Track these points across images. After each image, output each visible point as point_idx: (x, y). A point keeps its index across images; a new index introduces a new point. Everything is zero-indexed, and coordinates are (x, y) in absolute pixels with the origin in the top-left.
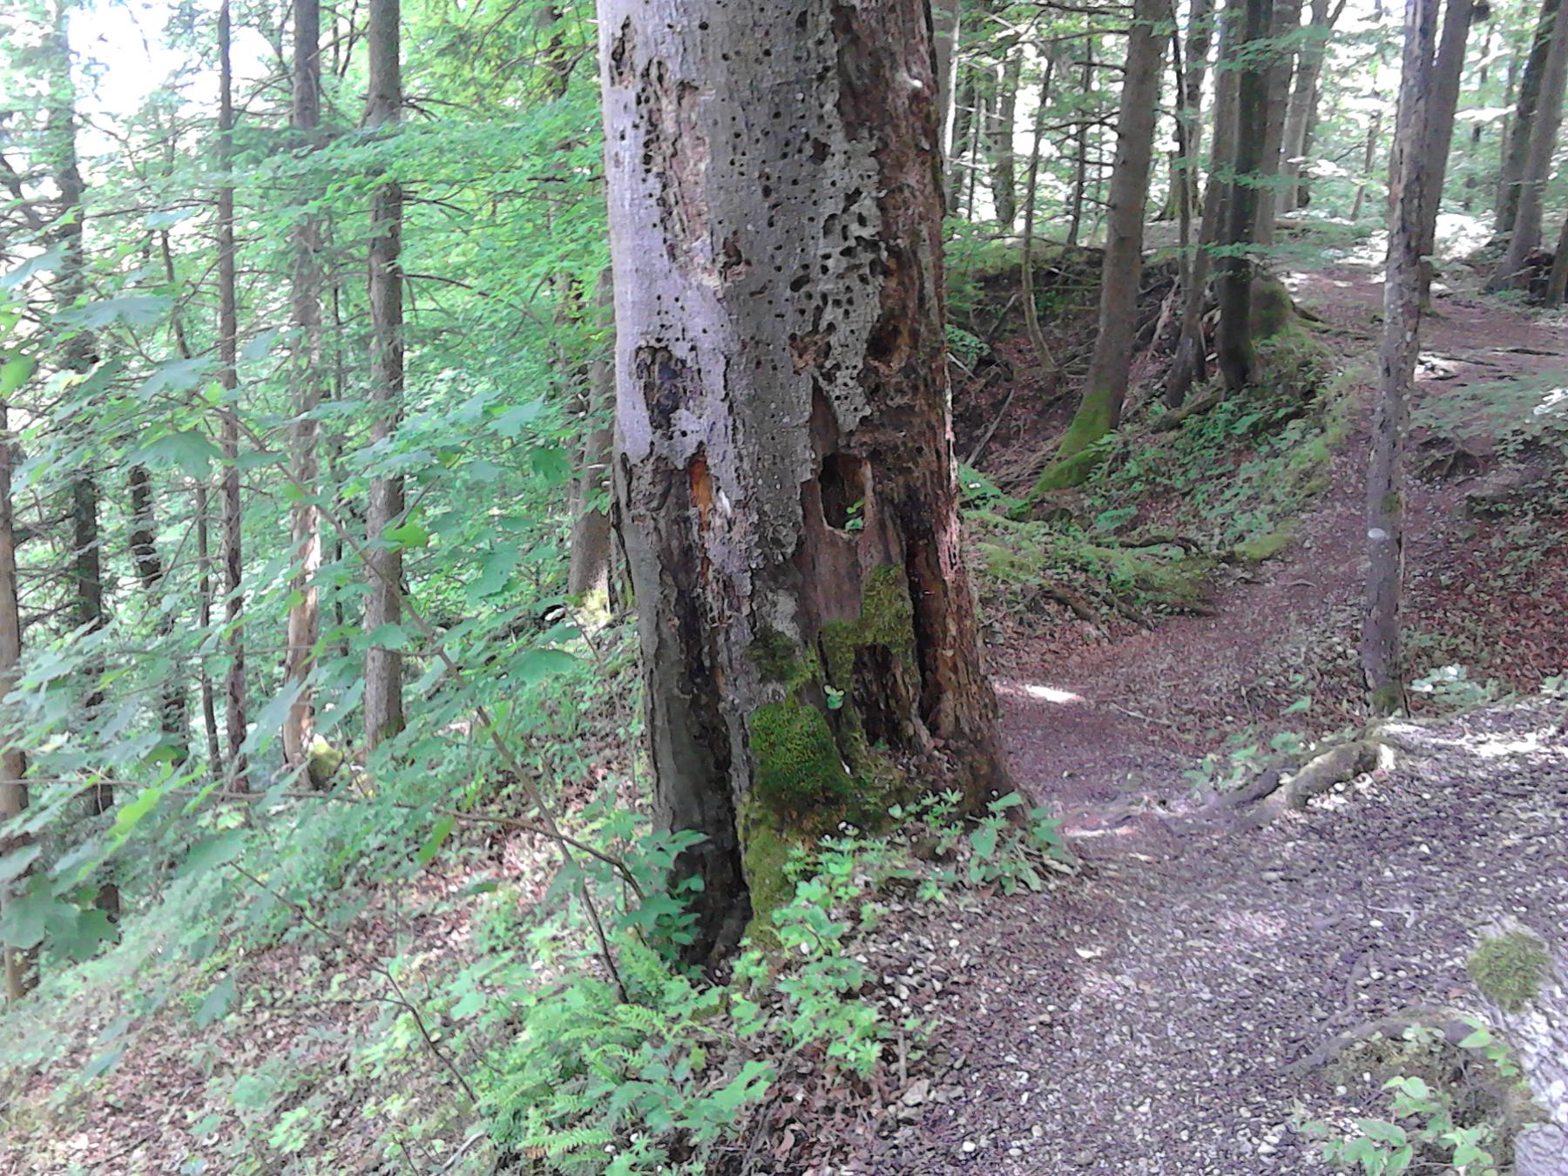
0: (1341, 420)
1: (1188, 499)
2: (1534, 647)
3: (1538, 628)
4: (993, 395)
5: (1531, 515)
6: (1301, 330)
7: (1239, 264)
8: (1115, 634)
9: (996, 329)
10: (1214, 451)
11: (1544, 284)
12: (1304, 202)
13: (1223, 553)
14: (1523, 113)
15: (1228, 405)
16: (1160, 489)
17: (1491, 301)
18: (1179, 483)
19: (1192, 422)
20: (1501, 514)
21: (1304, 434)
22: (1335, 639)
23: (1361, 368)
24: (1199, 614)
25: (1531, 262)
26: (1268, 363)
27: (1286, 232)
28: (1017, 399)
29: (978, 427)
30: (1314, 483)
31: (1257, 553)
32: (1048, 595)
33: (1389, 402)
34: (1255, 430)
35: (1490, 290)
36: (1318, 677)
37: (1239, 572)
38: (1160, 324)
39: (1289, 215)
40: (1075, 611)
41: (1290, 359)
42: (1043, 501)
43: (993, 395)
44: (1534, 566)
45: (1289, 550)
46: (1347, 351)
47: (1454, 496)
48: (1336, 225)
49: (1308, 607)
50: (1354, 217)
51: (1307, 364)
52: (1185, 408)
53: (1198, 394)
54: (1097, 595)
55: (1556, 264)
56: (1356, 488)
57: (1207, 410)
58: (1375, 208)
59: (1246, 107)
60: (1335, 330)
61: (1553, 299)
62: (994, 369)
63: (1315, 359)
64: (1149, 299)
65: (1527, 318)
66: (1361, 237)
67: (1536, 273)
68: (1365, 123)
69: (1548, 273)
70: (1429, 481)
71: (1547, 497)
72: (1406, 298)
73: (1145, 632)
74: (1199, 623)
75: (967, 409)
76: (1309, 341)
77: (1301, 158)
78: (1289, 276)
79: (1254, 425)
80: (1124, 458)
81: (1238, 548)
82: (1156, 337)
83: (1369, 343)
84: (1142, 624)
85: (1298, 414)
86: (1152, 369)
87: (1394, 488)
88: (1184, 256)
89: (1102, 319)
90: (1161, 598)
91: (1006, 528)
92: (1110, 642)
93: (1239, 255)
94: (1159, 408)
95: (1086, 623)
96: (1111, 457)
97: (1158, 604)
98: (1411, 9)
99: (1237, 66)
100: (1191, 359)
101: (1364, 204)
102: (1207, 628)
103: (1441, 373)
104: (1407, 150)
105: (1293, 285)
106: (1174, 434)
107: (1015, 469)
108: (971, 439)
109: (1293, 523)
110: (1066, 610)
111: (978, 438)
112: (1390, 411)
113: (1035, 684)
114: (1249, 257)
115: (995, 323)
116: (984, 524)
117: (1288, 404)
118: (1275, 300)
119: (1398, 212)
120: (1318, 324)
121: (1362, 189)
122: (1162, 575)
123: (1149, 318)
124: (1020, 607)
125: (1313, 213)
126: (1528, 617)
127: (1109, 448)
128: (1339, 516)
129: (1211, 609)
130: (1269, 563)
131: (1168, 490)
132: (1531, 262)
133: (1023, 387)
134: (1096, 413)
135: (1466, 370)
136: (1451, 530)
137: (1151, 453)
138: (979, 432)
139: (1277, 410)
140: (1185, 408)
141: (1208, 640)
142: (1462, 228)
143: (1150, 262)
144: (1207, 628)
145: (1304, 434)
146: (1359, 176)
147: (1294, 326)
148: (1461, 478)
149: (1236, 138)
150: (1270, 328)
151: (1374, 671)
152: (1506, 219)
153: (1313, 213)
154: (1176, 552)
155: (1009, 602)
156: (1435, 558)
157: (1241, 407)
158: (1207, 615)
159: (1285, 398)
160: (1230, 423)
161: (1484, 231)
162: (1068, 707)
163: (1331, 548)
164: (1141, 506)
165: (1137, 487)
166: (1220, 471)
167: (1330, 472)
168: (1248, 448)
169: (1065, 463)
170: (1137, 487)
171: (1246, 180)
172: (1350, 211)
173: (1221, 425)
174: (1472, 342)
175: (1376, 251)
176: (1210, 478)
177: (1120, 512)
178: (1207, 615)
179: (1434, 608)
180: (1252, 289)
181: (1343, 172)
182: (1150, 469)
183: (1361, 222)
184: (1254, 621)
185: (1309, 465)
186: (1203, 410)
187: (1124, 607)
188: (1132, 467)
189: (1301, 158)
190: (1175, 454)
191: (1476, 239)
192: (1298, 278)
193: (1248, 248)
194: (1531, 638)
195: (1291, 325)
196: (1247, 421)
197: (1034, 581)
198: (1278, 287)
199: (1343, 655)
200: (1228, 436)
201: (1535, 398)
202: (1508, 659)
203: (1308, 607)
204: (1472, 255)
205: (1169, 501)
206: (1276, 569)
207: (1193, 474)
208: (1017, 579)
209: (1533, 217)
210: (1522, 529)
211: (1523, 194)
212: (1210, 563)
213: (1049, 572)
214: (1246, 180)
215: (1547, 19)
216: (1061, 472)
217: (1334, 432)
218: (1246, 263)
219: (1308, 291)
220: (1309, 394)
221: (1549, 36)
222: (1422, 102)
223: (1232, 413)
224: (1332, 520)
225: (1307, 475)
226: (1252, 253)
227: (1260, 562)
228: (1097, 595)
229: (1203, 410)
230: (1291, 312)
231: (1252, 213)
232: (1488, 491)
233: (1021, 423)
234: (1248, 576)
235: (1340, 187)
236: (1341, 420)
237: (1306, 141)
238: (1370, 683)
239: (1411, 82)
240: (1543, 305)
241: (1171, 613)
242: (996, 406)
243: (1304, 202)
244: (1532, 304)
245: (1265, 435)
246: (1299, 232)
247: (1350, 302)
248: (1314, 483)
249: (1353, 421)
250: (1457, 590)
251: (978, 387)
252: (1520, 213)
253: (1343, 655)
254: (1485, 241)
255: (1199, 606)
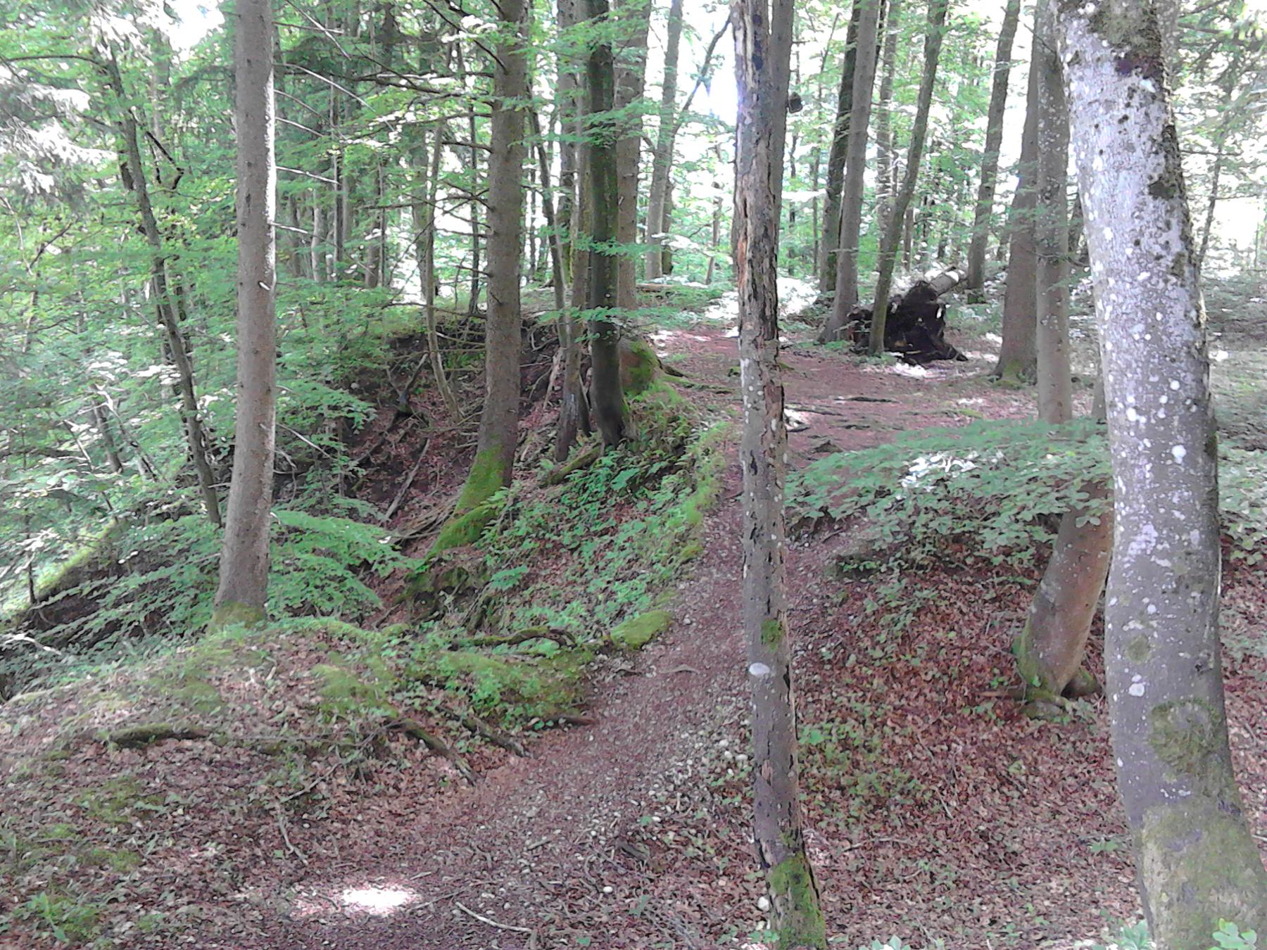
0: (710, 480)
1: (576, 554)
2: (920, 722)
3: (921, 698)
4: (411, 444)
5: (897, 571)
6: (668, 386)
7: (604, 328)
8: (477, 768)
9: (411, 385)
10: (598, 505)
11: (864, 335)
12: (668, 270)
13: (601, 642)
14: (833, 195)
15: (607, 461)
16: (549, 545)
17: (824, 351)
18: (566, 538)
19: (577, 476)
20: (869, 572)
21: (676, 491)
22: (723, 743)
23: (723, 423)
24: (576, 723)
25: (853, 317)
26: (641, 419)
27: (654, 295)
28: (434, 447)
29: (399, 474)
30: (691, 547)
31: (637, 638)
32: (394, 727)
33: (759, 507)
34: (633, 484)
35: (822, 341)
36: (708, 798)
37: (619, 663)
38: (553, 377)
39: (657, 280)
40: (429, 745)
41: (659, 414)
42: (440, 560)
43: (411, 444)
44: (908, 628)
45: (669, 629)
46: (710, 406)
47: (824, 554)
48: (694, 288)
49: (692, 701)
50: (708, 281)
51: (675, 419)
52: (570, 462)
53: (583, 448)
54: (457, 718)
55: (874, 317)
56: (730, 550)
57: (588, 465)
58: (723, 274)
59: (598, 180)
60: (697, 385)
61: (875, 348)
62: (411, 421)
63: (682, 415)
64: (541, 356)
65: (856, 365)
66: (714, 298)
67: (857, 327)
68: (712, 209)
69: (867, 326)
70: (798, 539)
71: (908, 552)
72: (767, 376)
73: (513, 760)
74: (575, 736)
75: (389, 458)
76: (676, 397)
77: (661, 235)
78: (656, 333)
79: (632, 480)
80: (515, 514)
81: (617, 631)
82: (550, 388)
83: (728, 396)
84: (509, 748)
85: (671, 469)
86: (548, 418)
87: (774, 611)
88: (561, 319)
89: (489, 379)
90: (531, 712)
91: (353, 640)
92: (470, 783)
93: (602, 317)
94: (547, 464)
95: (442, 760)
96: (503, 513)
97: (528, 719)
98: (740, 34)
99: (582, 139)
100: (574, 413)
101: (715, 271)
102: (585, 744)
103: (796, 425)
104: (750, 201)
105: (661, 341)
106: (561, 488)
107: (434, 511)
108: (393, 485)
109: (671, 594)
110: (417, 746)
111: (400, 484)
112: (760, 517)
113: (358, 885)
114: (614, 320)
115: (410, 379)
116: (327, 637)
117: (661, 459)
118: (641, 358)
119: (747, 276)
120: (683, 380)
121: (712, 259)
122: (532, 683)
123: (543, 372)
124: (357, 754)
125: (676, 279)
126: (910, 688)
127: (501, 505)
128: (717, 583)
129: (589, 717)
130: (649, 647)
131: (558, 546)
132: (853, 317)
133: (438, 436)
134: (489, 470)
135: (817, 421)
136: (825, 593)
137: (539, 509)
138: (400, 479)
139: (652, 464)
140: (570, 462)
141: (585, 760)
142: (794, 289)
143: (540, 323)
144: (585, 744)
145: (676, 491)
146: (709, 249)
147: (662, 382)
148: (827, 535)
149: (591, 209)
150: (640, 384)
151: (772, 844)
152: (828, 282)
153: (676, 279)
154: (547, 646)
155: (343, 748)
156: (813, 627)
157: (619, 461)
158: (584, 723)
159: (658, 452)
160: (610, 478)
161: (812, 292)
162: (406, 916)
163: (712, 622)
164: (532, 564)
165: (528, 545)
166: (604, 526)
167: (705, 535)
168: (628, 502)
169: (462, 519)
170: (528, 545)
171: (603, 247)
172: (705, 277)
173: (602, 478)
174: (817, 392)
175: (729, 308)
176: (595, 534)
177: (512, 572)
178: (584, 723)
179: (818, 689)
180: (619, 351)
181: (695, 245)
182: (539, 525)
183: (713, 285)
184: (636, 725)
185: (683, 528)
186: (586, 465)
187: (488, 730)
188: (522, 527)
189: (661, 235)
190: (562, 509)
191: (805, 298)
192: (664, 335)
193: (610, 312)
194: (916, 711)
195: (659, 381)
196: (624, 476)
197: (378, 714)
198: (643, 345)
199: (733, 764)
200: (609, 490)
201: (901, 469)
202: (899, 740)
203: (692, 701)
204: (804, 311)
205: (559, 557)
206: (657, 653)
207: (580, 531)
208: (356, 713)
209: (850, 280)
210: (891, 588)
211: (840, 260)
212: (587, 656)
213: (399, 697)
214: (603, 247)
215: (842, 119)
216: (458, 530)
217: (704, 492)
218: (611, 327)
219: (675, 348)
220: (679, 448)
221: (845, 133)
222: (762, 144)
223: (611, 467)
224: (710, 588)
225: (683, 539)
226: (616, 316)
227: (640, 648)
228: (457, 718)
229: (586, 465)
230: (657, 369)
231: (612, 279)
232: (854, 550)
233: (436, 469)
234: (627, 666)
235: (697, 258)
236: (710, 480)
237: (664, 221)
238: (769, 857)
239: (748, 121)
240: (866, 353)
241: (545, 728)
242: (415, 455)
243: (668, 270)
244: (858, 353)
245: (642, 489)
246: (664, 296)
247: (709, 355)
248: (691, 547)
249: (721, 480)
250: (839, 663)
251: (398, 437)
252: (839, 275)
253: (733, 764)
254: (812, 300)
255: (576, 715)
